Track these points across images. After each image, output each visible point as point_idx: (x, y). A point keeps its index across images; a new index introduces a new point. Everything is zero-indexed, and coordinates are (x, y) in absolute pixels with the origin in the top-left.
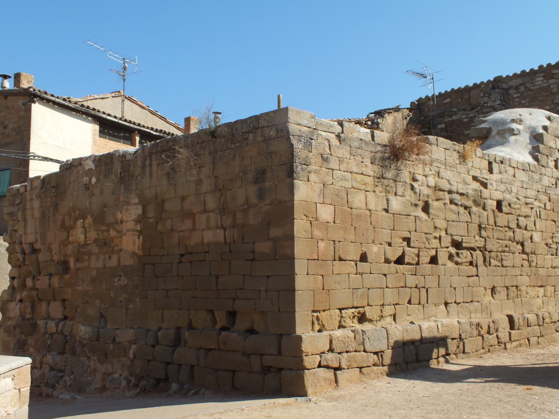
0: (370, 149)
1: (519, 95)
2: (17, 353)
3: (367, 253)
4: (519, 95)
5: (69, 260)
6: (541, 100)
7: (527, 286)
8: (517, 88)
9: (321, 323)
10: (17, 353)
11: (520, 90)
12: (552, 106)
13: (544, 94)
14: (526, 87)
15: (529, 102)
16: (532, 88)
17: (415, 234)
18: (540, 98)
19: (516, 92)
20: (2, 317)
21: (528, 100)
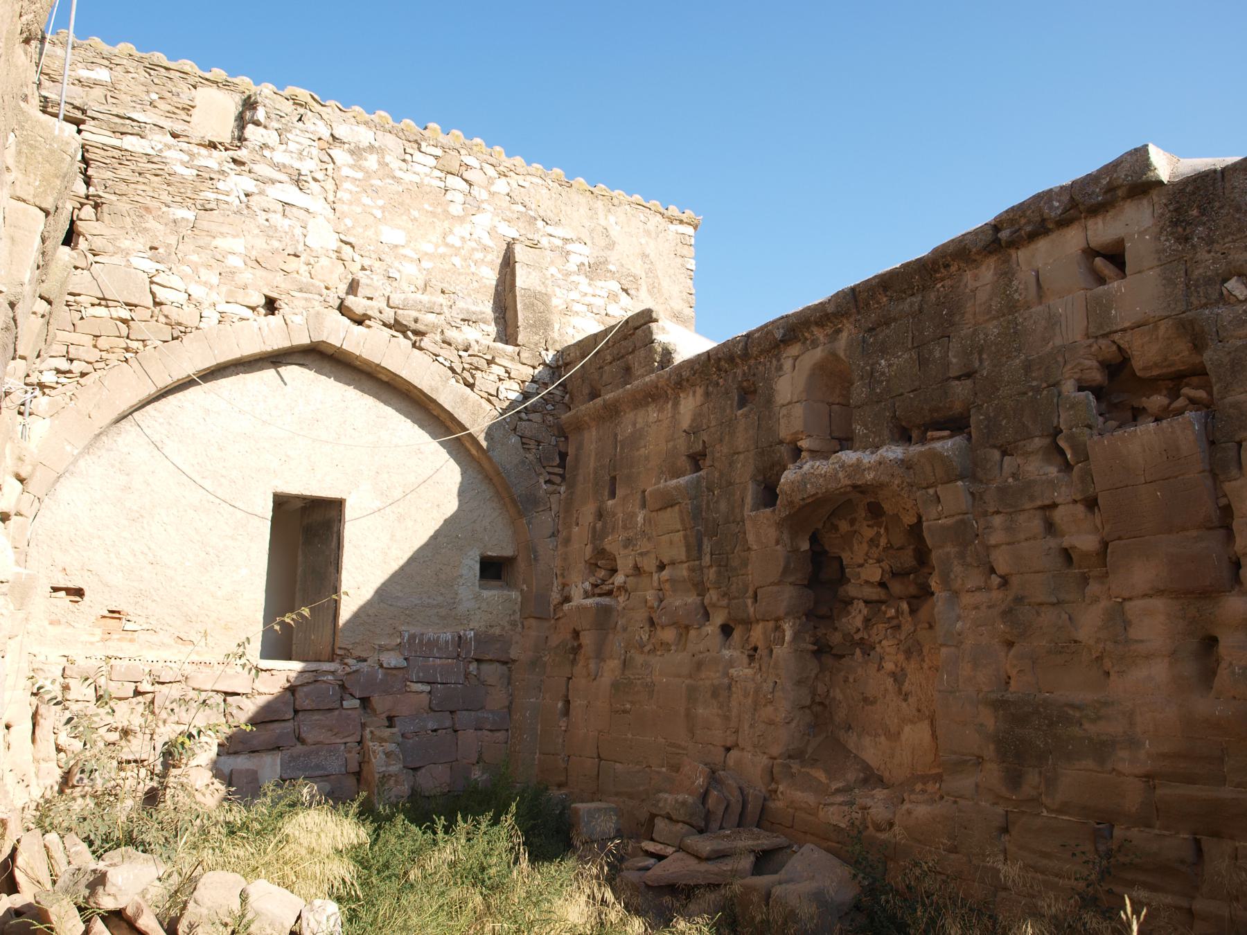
0: (125, 662)
1: (360, 175)
2: (600, 512)
3: (279, 490)
4: (360, 175)
5: (510, 586)
6: (415, 219)
7: (12, 305)
8: (356, 152)
9: (219, 146)
10: (600, 512)
11: (365, 164)
12: (442, 250)
13: (426, 206)
14: (383, 164)
15: (383, 208)
16: (399, 174)
17: (513, 414)
18: (415, 213)
19: (351, 162)
20: (451, 505)
21: (380, 202)
